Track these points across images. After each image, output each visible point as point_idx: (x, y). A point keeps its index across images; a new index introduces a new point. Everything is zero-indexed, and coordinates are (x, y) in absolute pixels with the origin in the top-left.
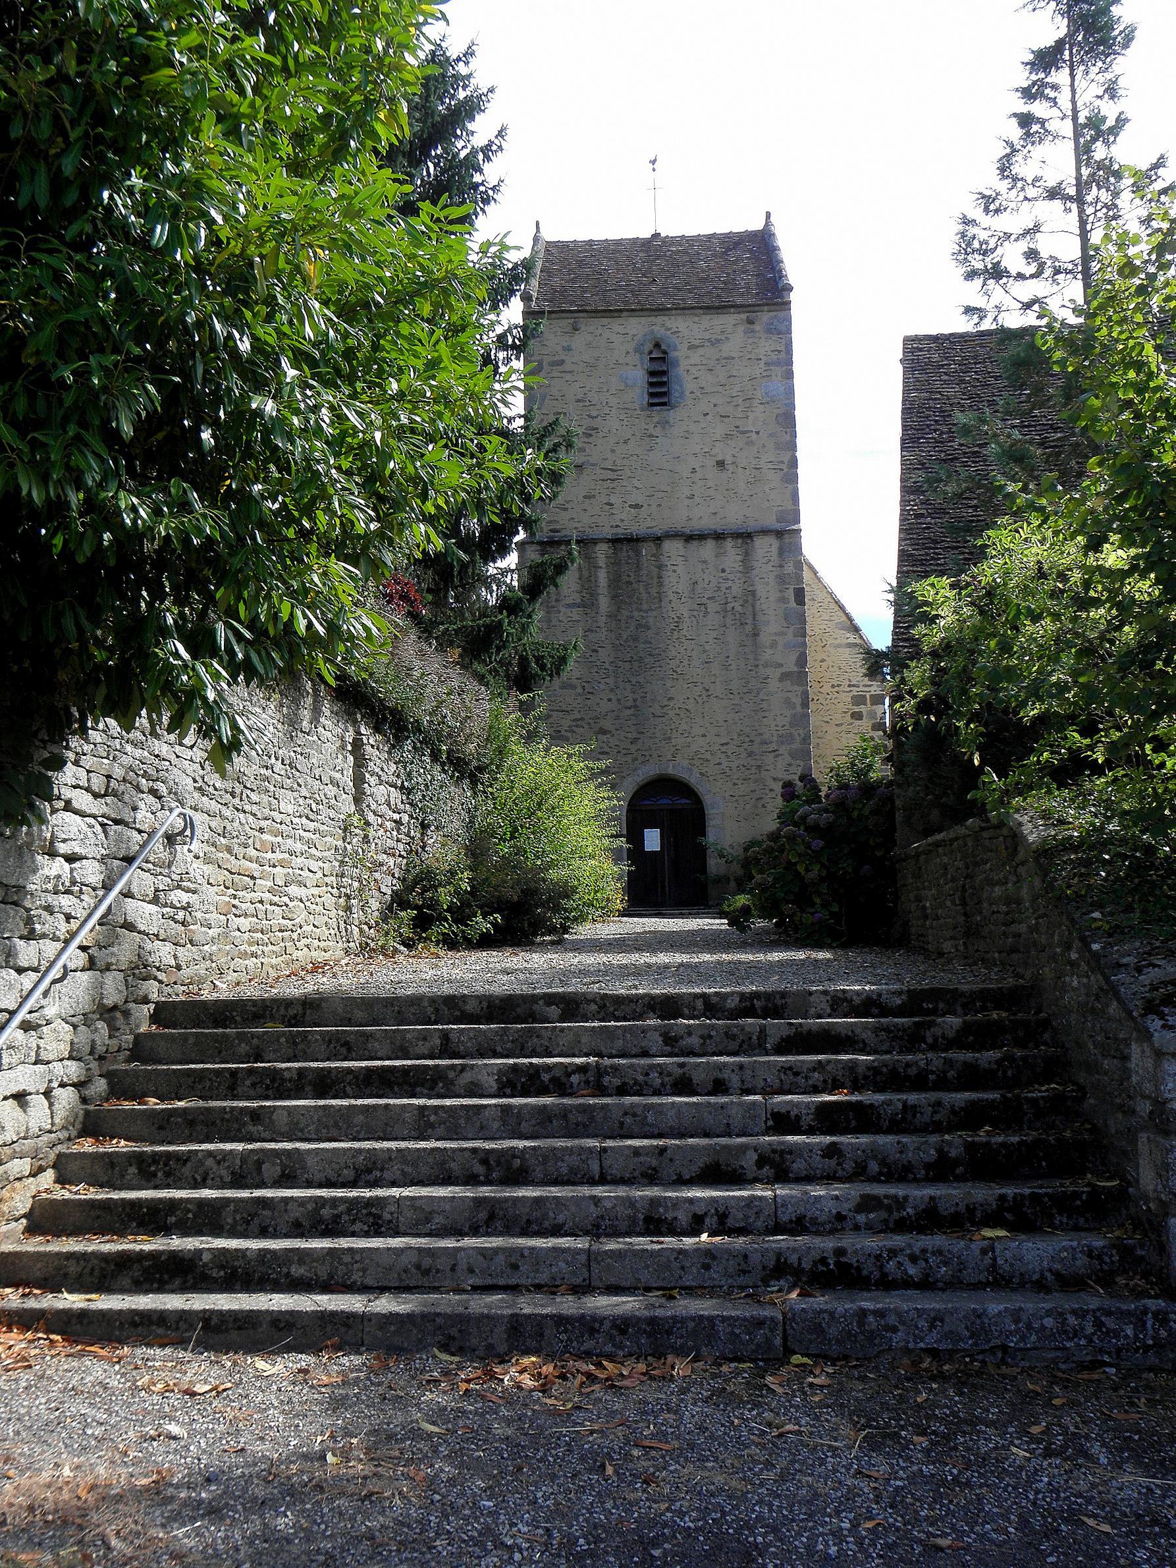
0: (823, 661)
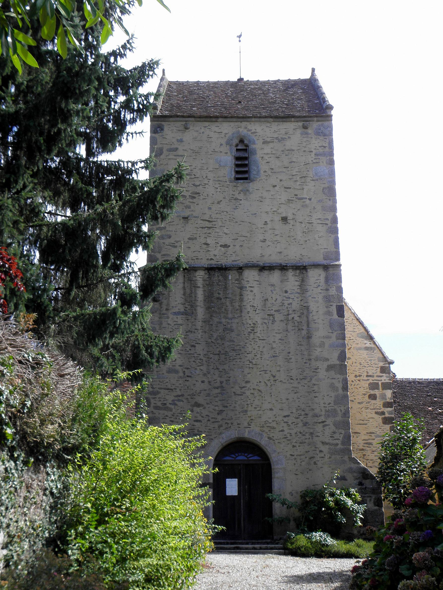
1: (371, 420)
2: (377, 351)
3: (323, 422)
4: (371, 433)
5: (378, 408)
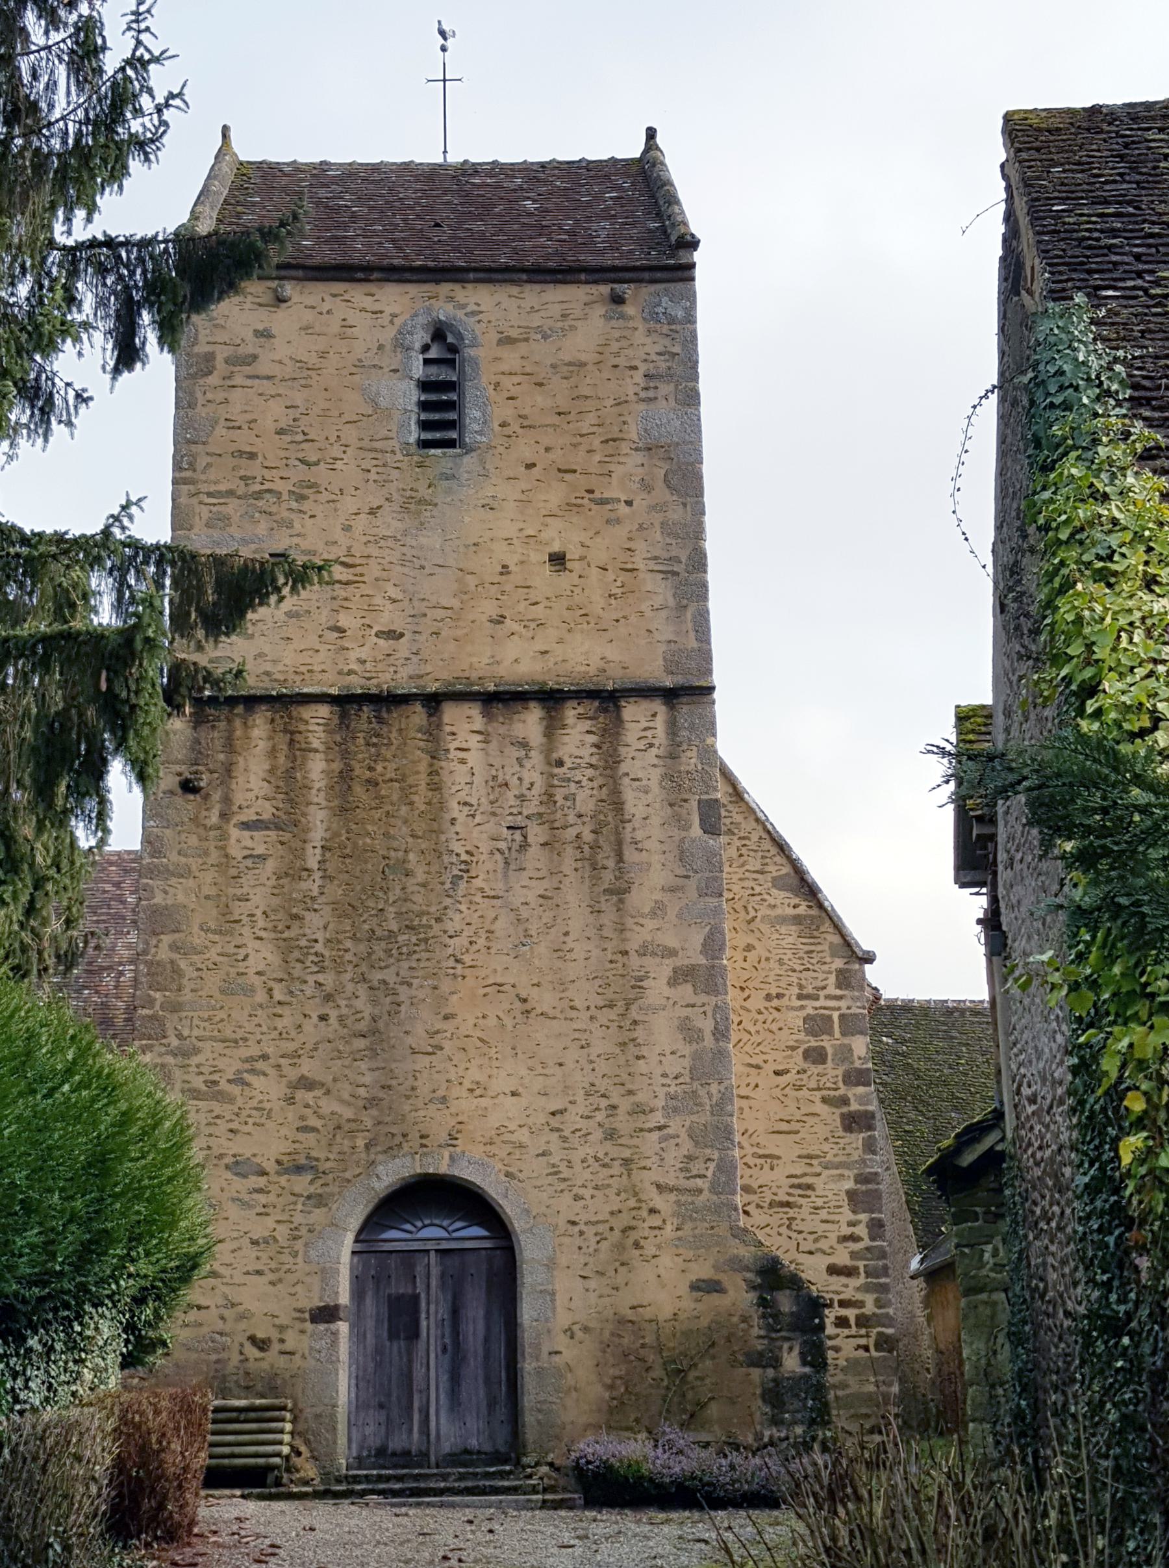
0: (749, 948)
1: (811, 1121)
2: (827, 926)
3: (660, 1128)
5: (828, 1085)
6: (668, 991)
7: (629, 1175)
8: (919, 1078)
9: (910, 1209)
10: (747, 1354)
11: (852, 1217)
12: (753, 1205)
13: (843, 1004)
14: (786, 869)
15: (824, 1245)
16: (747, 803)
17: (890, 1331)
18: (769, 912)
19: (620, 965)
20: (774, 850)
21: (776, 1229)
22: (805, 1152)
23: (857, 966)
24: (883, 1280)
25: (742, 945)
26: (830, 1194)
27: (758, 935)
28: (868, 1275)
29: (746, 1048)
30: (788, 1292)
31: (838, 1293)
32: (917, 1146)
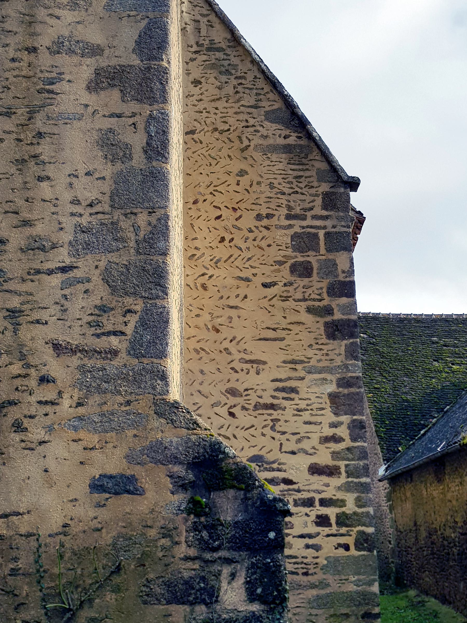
0: (242, 173)
1: (296, 329)
2: (315, 154)
3: (64, 270)
4: (293, 362)
5: (313, 296)
6: (86, 97)
7: (15, 332)
8: (383, 357)
9: (378, 436)
10: (168, 585)
11: (334, 419)
12: (239, 407)
13: (329, 223)
14: (278, 105)
15: (306, 445)
16: (243, 47)
17: (370, 530)
18: (261, 142)
19: (24, 64)
20: (267, 88)
21: (260, 430)
22: (289, 358)
23: (342, 190)
24: (364, 480)
25: (236, 170)
26: (313, 397)
27: (251, 161)
28: (349, 474)
29: (236, 263)
30: (231, 493)
31: (319, 492)
32: (383, 397)
